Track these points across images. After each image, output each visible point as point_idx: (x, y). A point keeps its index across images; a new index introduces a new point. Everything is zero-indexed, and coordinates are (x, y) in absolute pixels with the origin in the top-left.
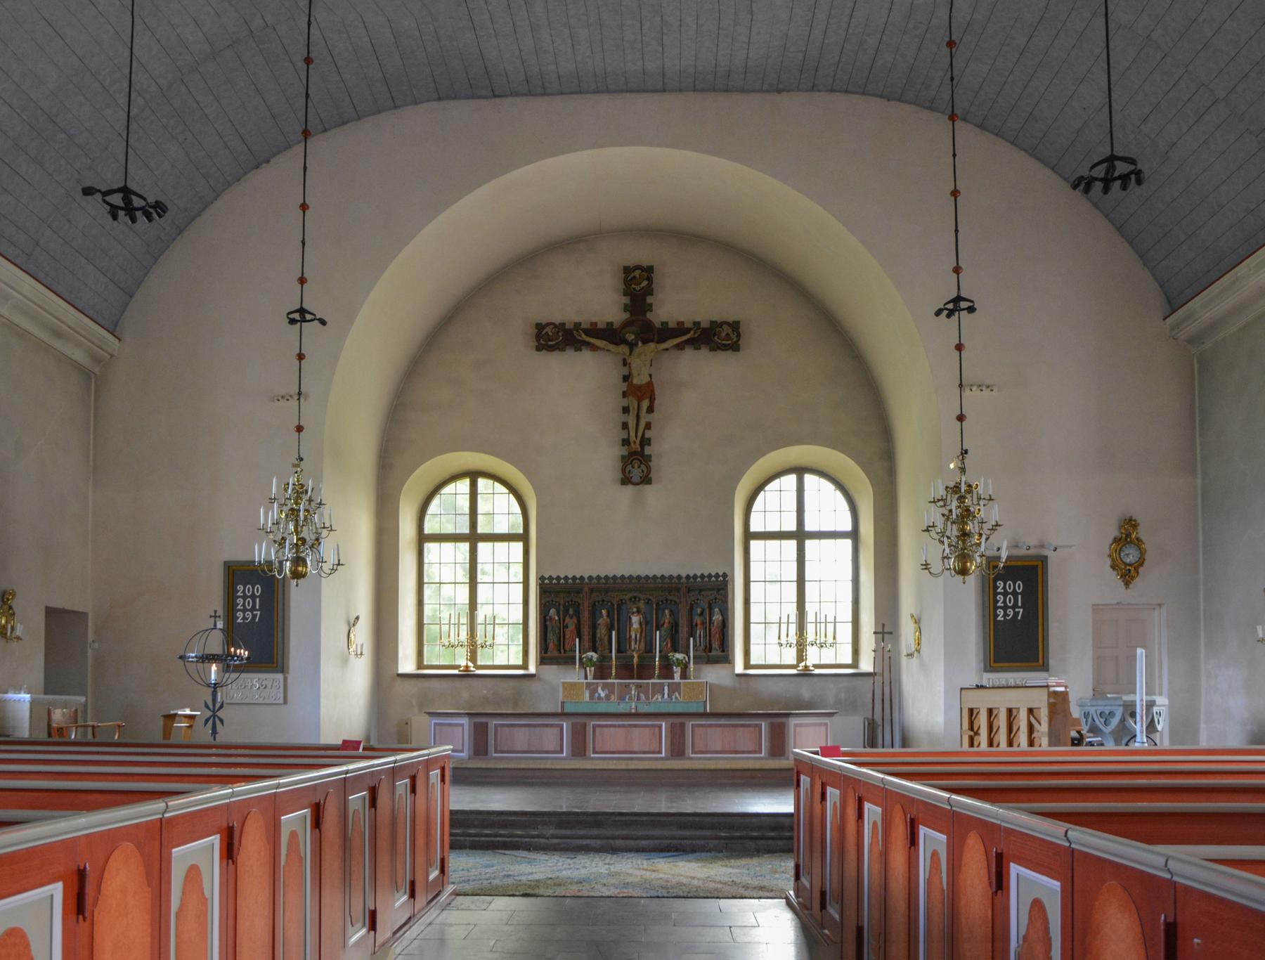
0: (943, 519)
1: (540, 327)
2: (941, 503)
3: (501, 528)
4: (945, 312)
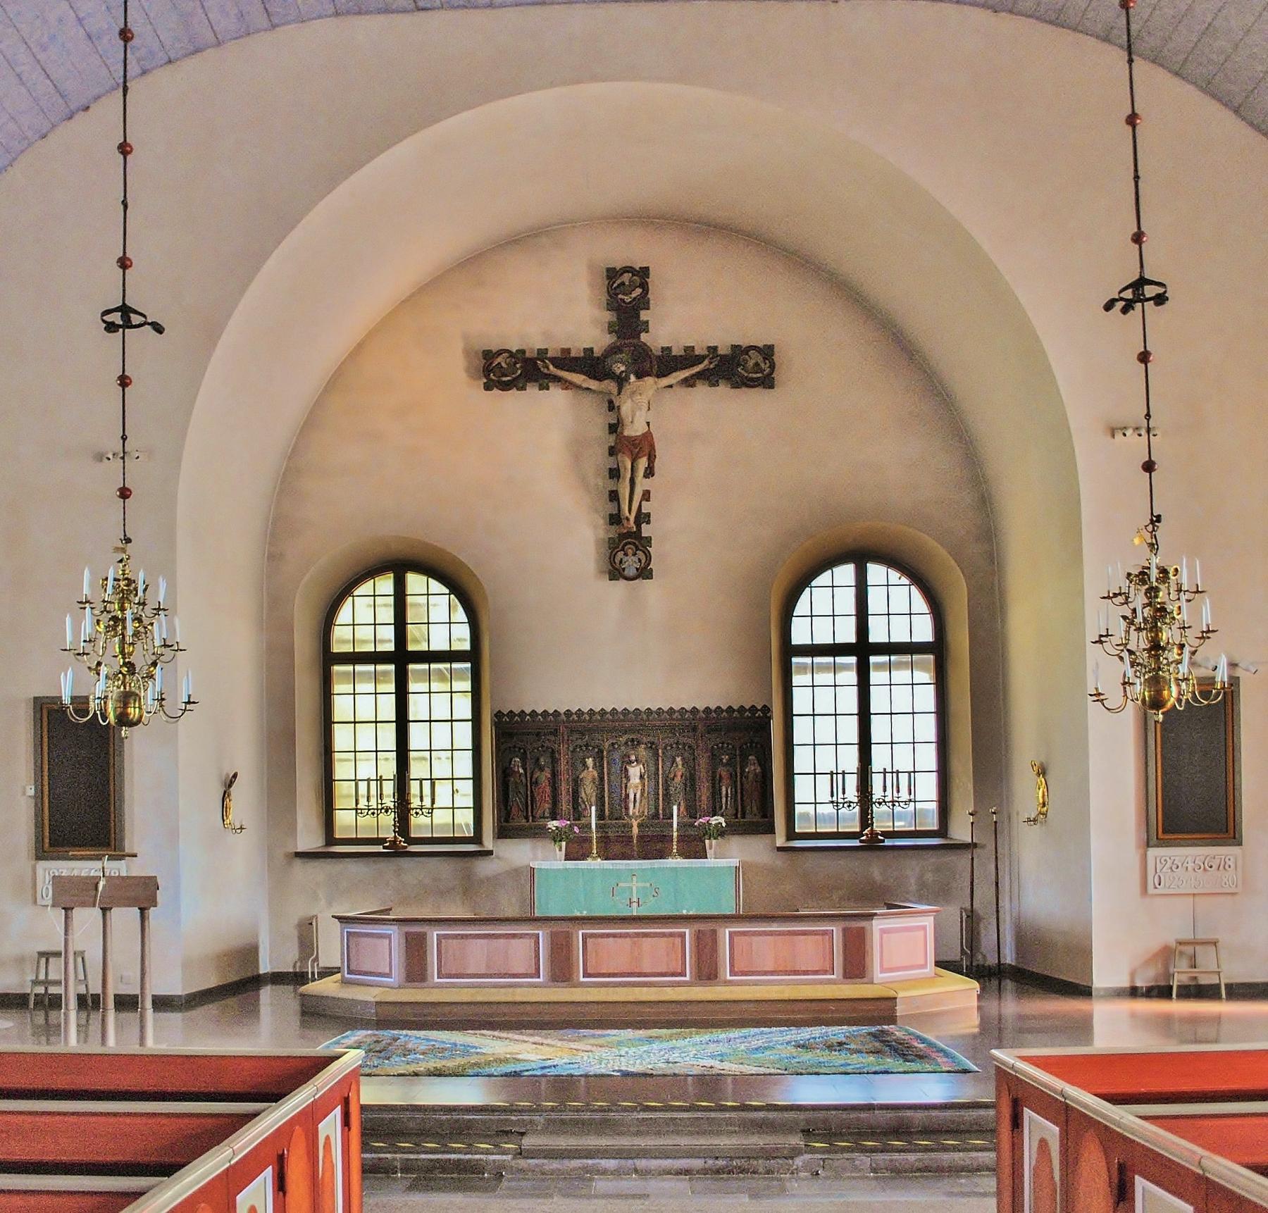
0: (1123, 624)
1: (488, 355)
2: (1121, 599)
3: (439, 643)
4: (1120, 304)
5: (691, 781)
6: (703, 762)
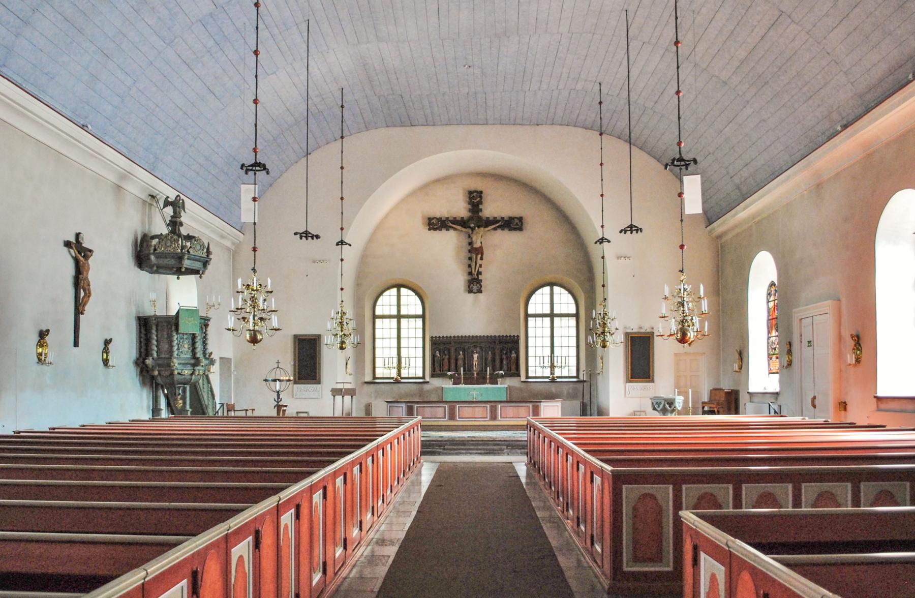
1: (430, 219)
5: (494, 360)
6: (497, 352)
